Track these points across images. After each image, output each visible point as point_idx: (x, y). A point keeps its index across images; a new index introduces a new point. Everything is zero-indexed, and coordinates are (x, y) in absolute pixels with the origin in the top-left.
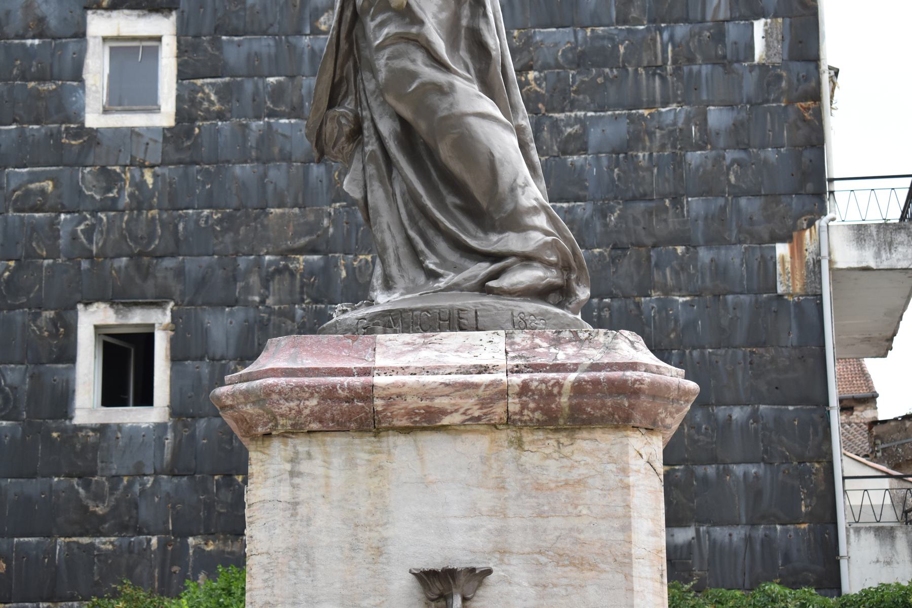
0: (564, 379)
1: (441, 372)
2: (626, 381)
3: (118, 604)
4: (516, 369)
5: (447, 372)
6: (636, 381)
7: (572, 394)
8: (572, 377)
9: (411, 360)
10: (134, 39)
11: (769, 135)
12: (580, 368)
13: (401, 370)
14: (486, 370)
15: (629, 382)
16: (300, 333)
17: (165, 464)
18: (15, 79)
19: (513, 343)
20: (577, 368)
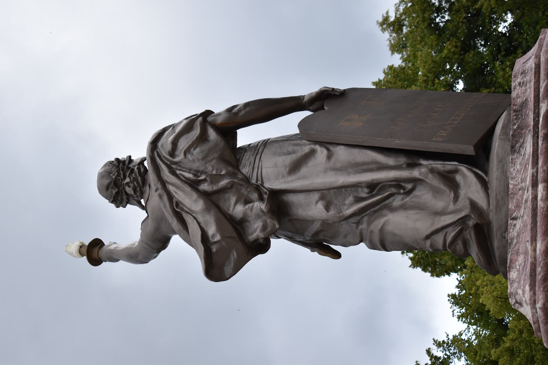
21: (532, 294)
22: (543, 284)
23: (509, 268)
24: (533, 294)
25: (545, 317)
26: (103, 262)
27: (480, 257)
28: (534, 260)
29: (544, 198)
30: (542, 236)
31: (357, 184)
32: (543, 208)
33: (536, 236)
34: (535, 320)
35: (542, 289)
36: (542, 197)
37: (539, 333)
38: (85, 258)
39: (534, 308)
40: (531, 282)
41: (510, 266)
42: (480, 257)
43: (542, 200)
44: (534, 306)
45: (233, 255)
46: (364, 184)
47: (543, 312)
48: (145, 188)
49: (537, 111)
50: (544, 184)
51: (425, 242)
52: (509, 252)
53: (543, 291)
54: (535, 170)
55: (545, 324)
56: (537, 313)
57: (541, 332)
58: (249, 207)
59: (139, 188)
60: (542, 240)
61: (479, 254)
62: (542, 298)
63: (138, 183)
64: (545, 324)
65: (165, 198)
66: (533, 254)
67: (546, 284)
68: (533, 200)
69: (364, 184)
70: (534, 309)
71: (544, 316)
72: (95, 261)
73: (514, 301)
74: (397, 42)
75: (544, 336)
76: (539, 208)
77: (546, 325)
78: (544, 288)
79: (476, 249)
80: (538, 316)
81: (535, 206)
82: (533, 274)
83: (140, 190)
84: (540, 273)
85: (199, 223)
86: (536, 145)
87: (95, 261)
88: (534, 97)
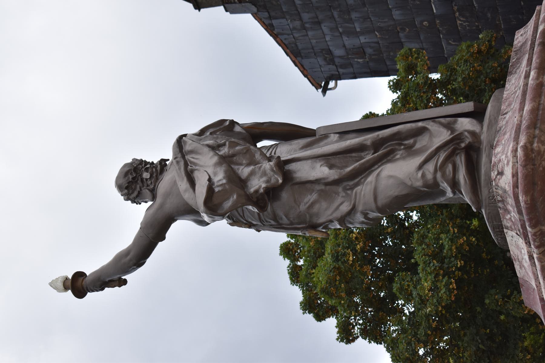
0: (531, 232)
1: (536, 273)
2: (528, 219)
3: (391, 230)
4: (528, 244)
5: (536, 271)
6: (525, 203)
7: (539, 225)
8: (529, 229)
9: (526, 262)
10: (160, 182)
11: (454, 211)
12: (522, 218)
13: (539, 288)
14: (532, 256)
15: (527, 206)
16: (415, 110)
17: (322, 163)
18: (410, 329)
19: (511, 227)
20: (523, 220)
21: (515, 144)
22: (526, 130)
23: (495, 147)
24: (516, 144)
25: (525, 158)
26: (87, 293)
27: (467, 179)
28: (519, 122)
29: (534, 78)
30: (526, 130)
31: (363, 141)
32: (533, 84)
33: (525, 102)
34: (514, 173)
35: (525, 134)
36: (533, 78)
37: (517, 190)
38: (70, 291)
39: (515, 156)
40: (515, 136)
41: (496, 144)
42: (467, 179)
43: (532, 80)
44: (515, 154)
45: (233, 197)
46: (369, 140)
47: (524, 151)
48: (160, 176)
49: (535, 35)
50: (535, 70)
51: (417, 174)
52: (497, 136)
53: (525, 135)
54: (528, 68)
55: (524, 167)
56: (517, 162)
57: (518, 188)
58: (258, 166)
59: (156, 174)
60: (529, 103)
61: (466, 176)
62: (524, 139)
63: (156, 170)
64: (524, 167)
65: (182, 163)
66: (520, 118)
67: (529, 131)
68: (524, 86)
69: (369, 140)
70: (515, 158)
71: (524, 157)
72: (80, 293)
73: (496, 173)
74: (406, 154)
75: (521, 184)
76: (529, 84)
77: (524, 168)
78: (527, 133)
79: (464, 172)
80: (518, 167)
81: (525, 89)
82: (518, 131)
83: (157, 176)
84: (524, 124)
85: (208, 173)
86: (531, 54)
87: (80, 293)
88: (534, 28)
